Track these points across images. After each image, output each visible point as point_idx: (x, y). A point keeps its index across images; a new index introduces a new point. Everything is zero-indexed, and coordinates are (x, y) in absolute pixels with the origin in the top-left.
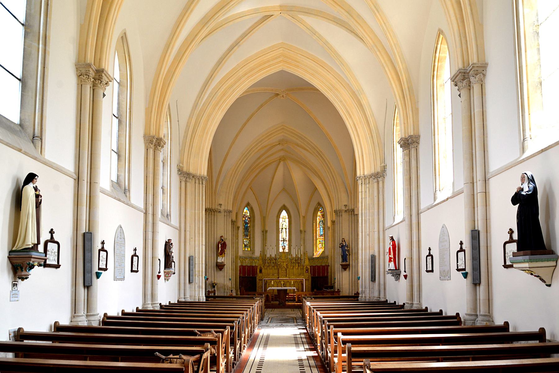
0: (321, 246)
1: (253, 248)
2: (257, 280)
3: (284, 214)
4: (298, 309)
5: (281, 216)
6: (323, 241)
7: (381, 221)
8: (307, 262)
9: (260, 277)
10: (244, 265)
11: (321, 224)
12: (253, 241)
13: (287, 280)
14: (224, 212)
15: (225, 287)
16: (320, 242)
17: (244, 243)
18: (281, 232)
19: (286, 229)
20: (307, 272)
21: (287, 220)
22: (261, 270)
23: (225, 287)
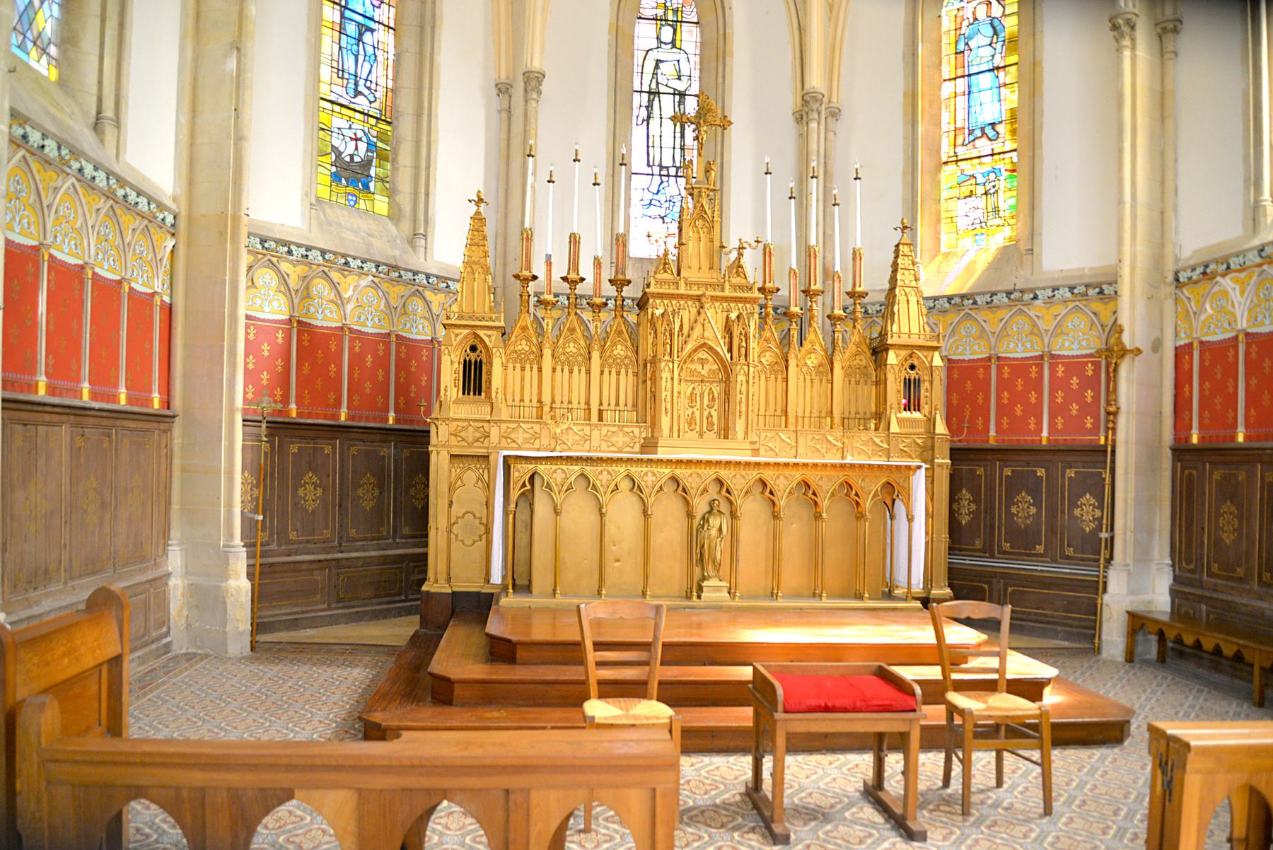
0: (979, 214)
1: (416, 195)
2: (439, 462)
9: (470, 434)
10: (325, 317)
12: (418, 142)
18: (644, 113)
22: (479, 365)
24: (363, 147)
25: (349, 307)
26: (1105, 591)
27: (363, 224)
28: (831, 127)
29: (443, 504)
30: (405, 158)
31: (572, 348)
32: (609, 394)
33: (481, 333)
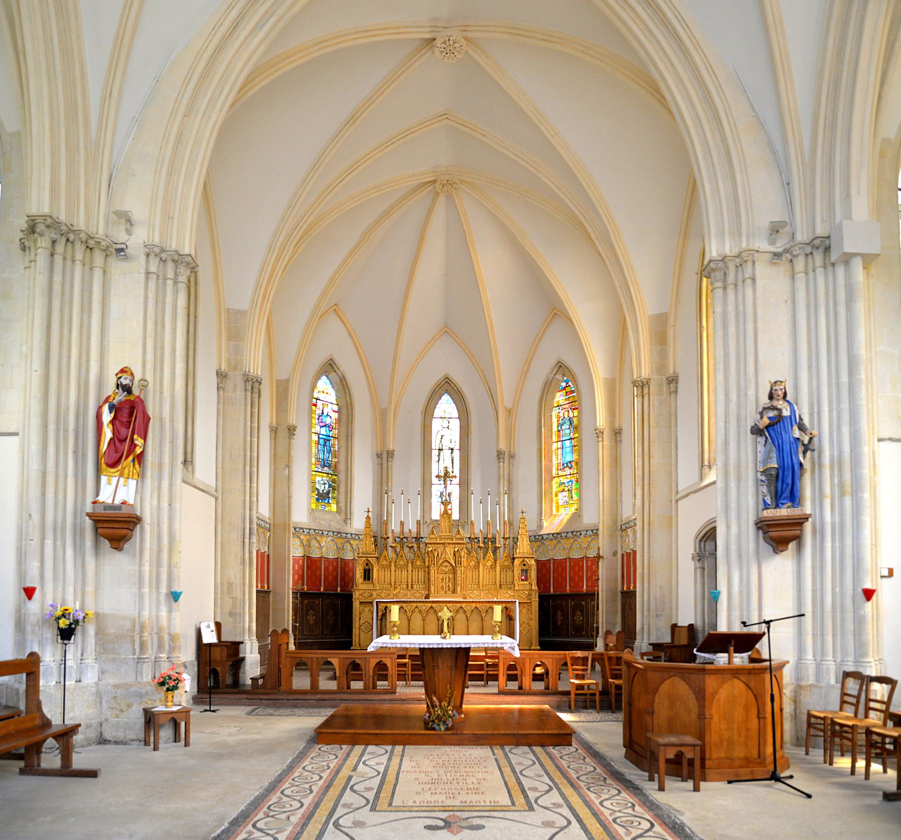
0: (566, 499)
1: (346, 503)
2: (356, 604)
3: (446, 406)
4: (526, 749)
5: (438, 413)
6: (571, 481)
7: (731, 435)
8: (524, 547)
9: (366, 595)
10: (315, 554)
11: (568, 431)
13: (459, 605)
14: (148, 255)
15: (141, 637)
16: (562, 488)
17: (317, 486)
19: (452, 449)
20: (526, 579)
21: (456, 424)
22: (369, 570)
23: (141, 637)
24: (327, 486)
25: (324, 549)
26: (596, 646)
27: (327, 517)
28: (511, 462)
29: (357, 619)
30: (342, 489)
31: (402, 563)
32: (415, 579)
33: (370, 559)
